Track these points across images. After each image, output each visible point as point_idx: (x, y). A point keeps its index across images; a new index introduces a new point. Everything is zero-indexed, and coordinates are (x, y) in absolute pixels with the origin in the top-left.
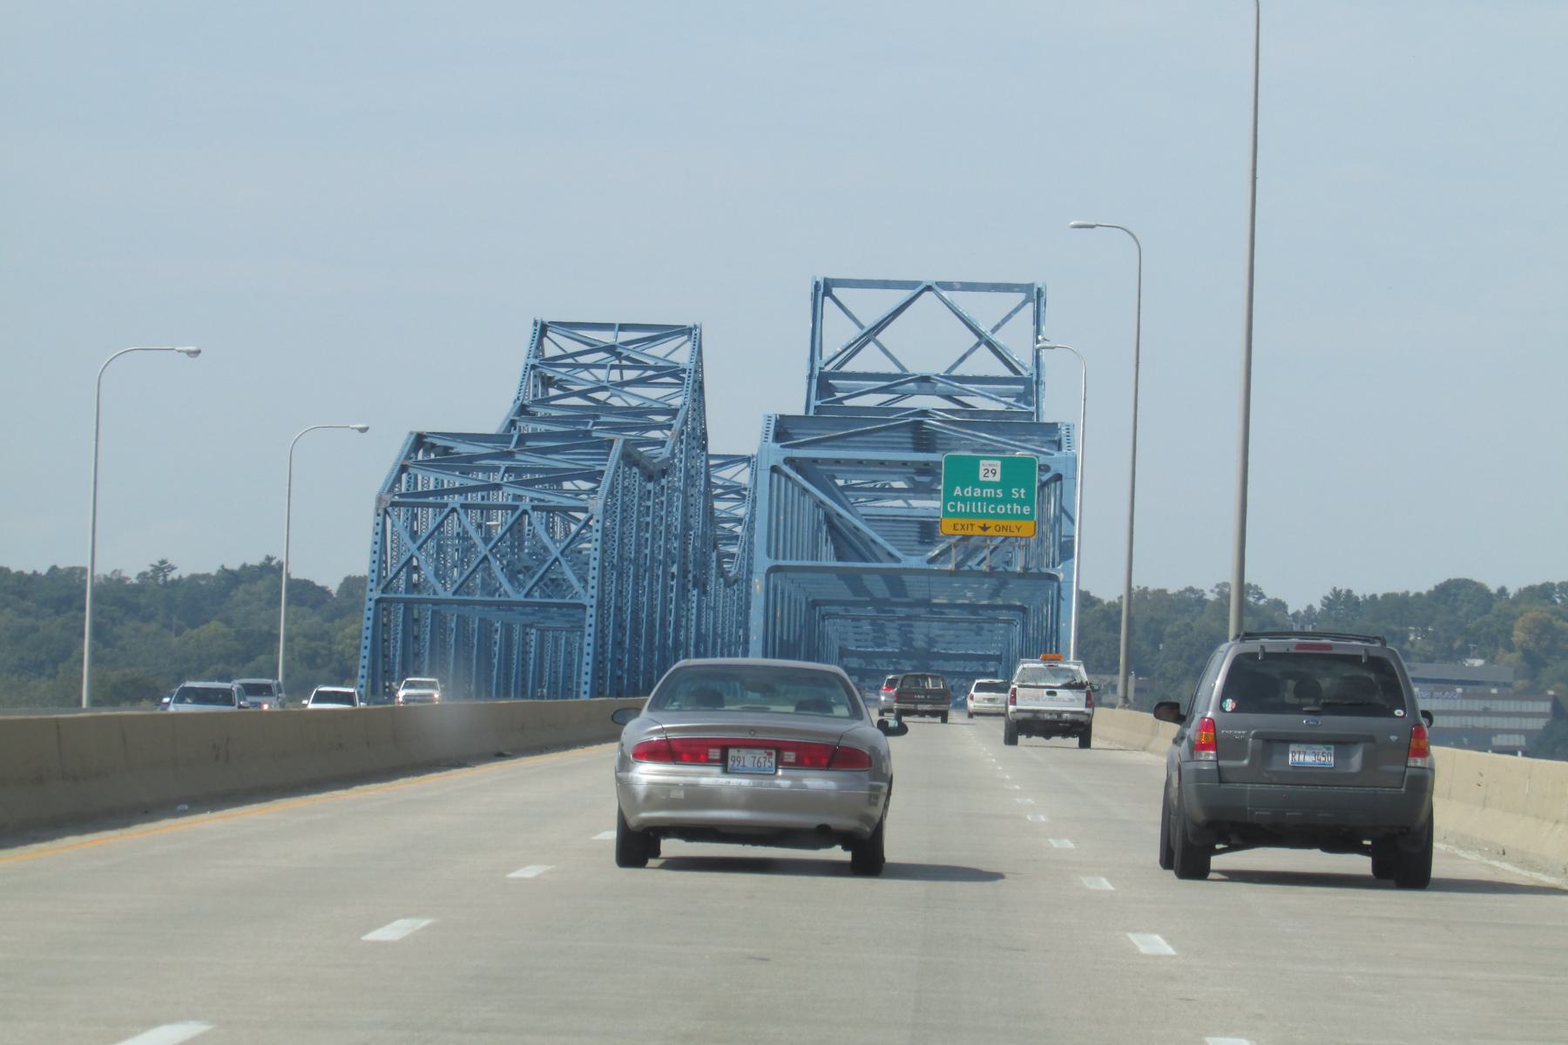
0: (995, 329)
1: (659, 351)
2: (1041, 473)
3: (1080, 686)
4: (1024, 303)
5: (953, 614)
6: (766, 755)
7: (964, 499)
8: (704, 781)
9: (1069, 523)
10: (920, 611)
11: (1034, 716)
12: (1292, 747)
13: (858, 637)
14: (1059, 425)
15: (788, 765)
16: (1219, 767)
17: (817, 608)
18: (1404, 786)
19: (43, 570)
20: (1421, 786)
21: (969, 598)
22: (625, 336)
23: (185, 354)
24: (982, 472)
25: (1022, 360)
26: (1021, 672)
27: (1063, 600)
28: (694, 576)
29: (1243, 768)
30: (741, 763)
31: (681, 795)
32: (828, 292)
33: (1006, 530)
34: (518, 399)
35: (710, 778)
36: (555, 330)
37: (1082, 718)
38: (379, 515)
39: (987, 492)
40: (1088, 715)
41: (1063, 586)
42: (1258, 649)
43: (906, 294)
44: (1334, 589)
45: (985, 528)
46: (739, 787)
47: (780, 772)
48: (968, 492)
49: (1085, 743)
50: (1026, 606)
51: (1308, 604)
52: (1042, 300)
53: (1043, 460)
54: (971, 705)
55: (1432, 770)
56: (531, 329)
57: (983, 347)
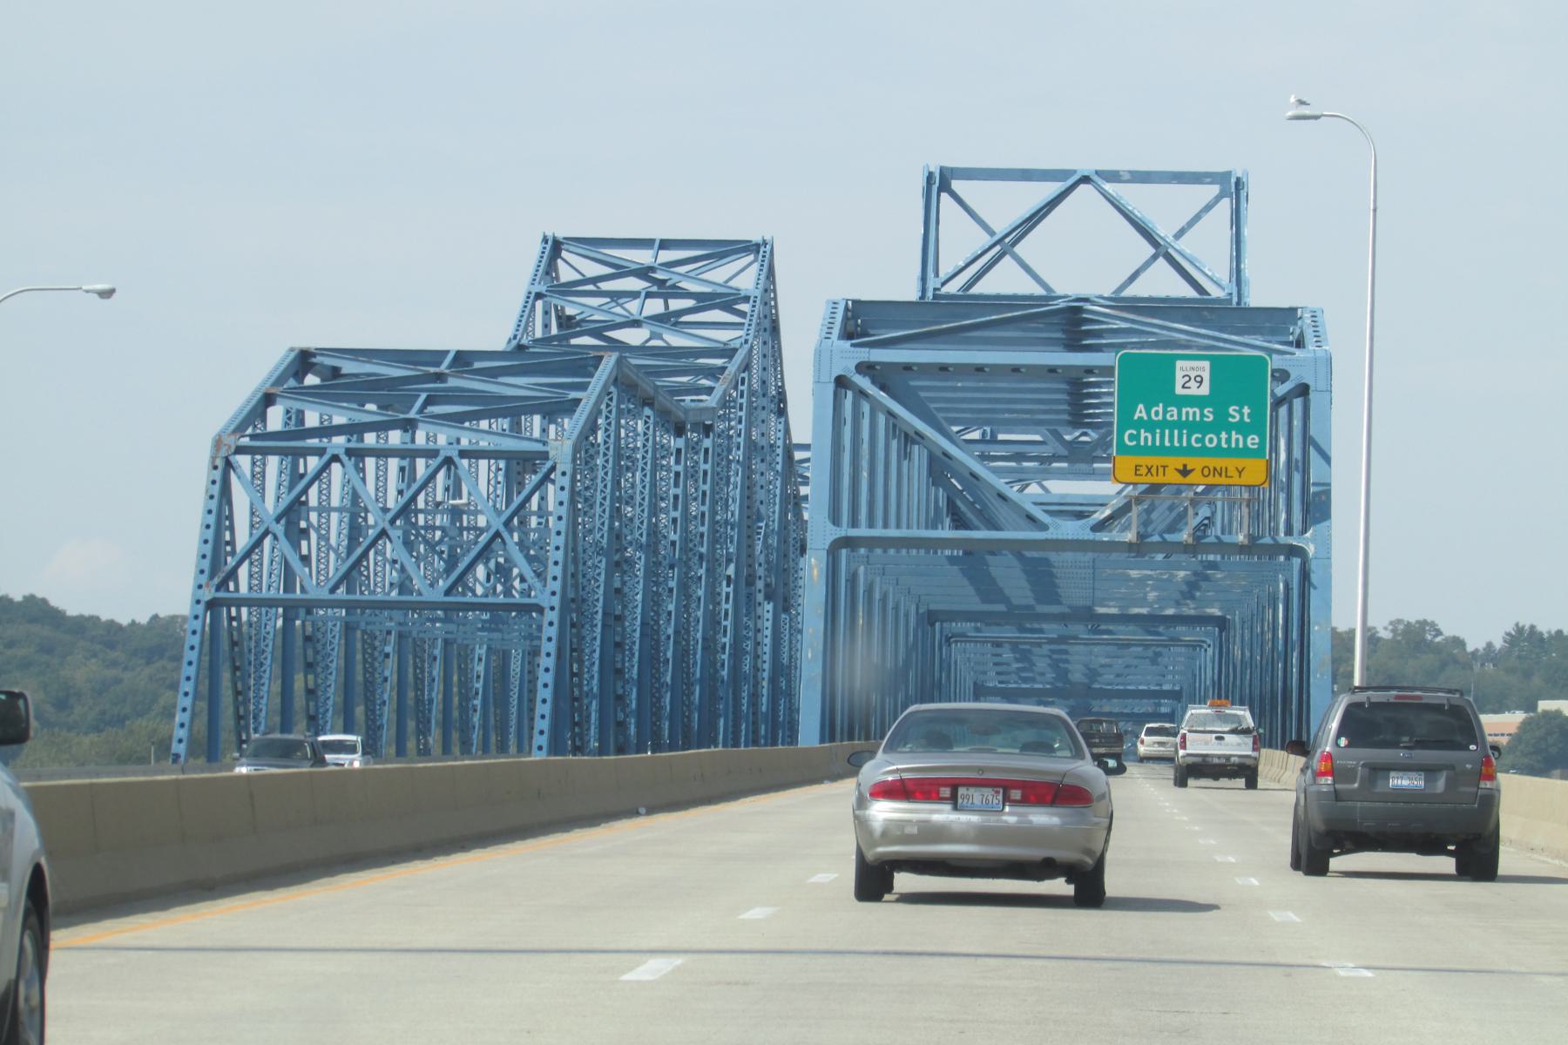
0: (1180, 234)
1: (720, 274)
2: (1275, 383)
3: (1246, 732)
4: (1217, 199)
5: (1125, 633)
6: (993, 793)
7: (1150, 426)
8: (936, 817)
9: (1323, 462)
10: (1079, 629)
11: (1204, 760)
12: (1392, 774)
13: (1000, 669)
14: (1299, 311)
15: (1014, 803)
16: (1335, 791)
17: (937, 624)
18: (1477, 802)
19: (143, 619)
20: (1489, 803)
21: (1150, 605)
22: (667, 256)
23: (96, 296)
24: (1179, 381)
25: (1217, 275)
26: (1189, 717)
27: (1315, 588)
28: (767, 585)
29: (1354, 791)
30: (970, 801)
31: (915, 830)
32: (945, 187)
33: (1220, 475)
34: (515, 337)
35: (941, 814)
36: (572, 248)
37: (1248, 762)
38: (215, 468)
39: (1187, 413)
40: (1255, 759)
41: (1314, 565)
42: (1364, 700)
43: (1052, 189)
44: (1517, 625)
45: (1185, 472)
46: (969, 823)
47: (1007, 809)
48: (1157, 413)
49: (1252, 784)
50: (1228, 617)
51: (1488, 640)
52: (1243, 194)
53: (1276, 362)
54: (1142, 749)
55: (1499, 791)
56: (537, 247)
57: (1161, 260)
